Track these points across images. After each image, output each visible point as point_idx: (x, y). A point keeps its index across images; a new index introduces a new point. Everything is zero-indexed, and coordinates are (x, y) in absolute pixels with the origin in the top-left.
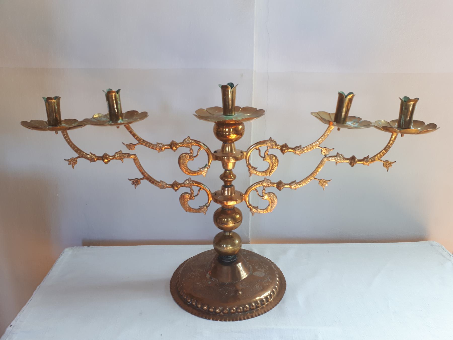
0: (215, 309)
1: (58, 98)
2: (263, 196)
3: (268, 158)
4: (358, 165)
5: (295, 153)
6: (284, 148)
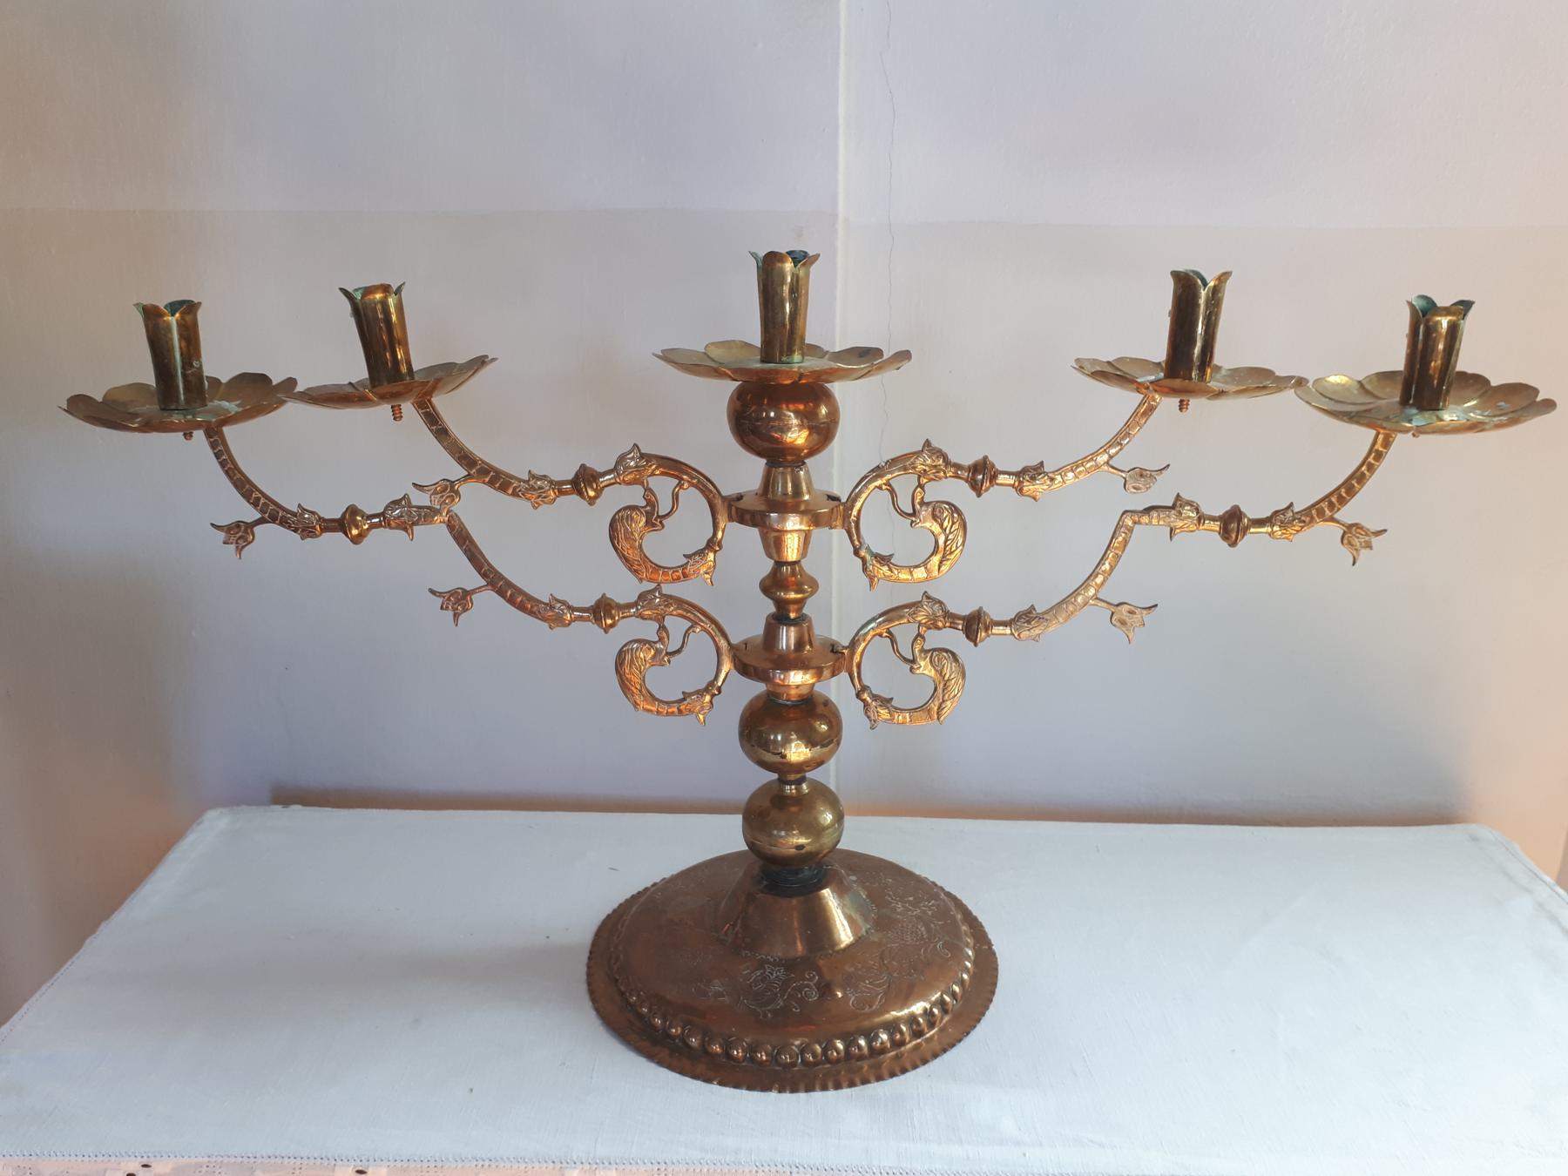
0: (752, 1049)
1: (188, 308)
2: (913, 661)
3: (925, 513)
4: (1257, 536)
5: (1020, 490)
6: (981, 474)
